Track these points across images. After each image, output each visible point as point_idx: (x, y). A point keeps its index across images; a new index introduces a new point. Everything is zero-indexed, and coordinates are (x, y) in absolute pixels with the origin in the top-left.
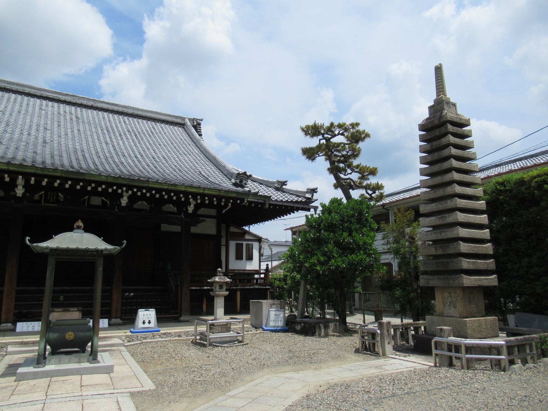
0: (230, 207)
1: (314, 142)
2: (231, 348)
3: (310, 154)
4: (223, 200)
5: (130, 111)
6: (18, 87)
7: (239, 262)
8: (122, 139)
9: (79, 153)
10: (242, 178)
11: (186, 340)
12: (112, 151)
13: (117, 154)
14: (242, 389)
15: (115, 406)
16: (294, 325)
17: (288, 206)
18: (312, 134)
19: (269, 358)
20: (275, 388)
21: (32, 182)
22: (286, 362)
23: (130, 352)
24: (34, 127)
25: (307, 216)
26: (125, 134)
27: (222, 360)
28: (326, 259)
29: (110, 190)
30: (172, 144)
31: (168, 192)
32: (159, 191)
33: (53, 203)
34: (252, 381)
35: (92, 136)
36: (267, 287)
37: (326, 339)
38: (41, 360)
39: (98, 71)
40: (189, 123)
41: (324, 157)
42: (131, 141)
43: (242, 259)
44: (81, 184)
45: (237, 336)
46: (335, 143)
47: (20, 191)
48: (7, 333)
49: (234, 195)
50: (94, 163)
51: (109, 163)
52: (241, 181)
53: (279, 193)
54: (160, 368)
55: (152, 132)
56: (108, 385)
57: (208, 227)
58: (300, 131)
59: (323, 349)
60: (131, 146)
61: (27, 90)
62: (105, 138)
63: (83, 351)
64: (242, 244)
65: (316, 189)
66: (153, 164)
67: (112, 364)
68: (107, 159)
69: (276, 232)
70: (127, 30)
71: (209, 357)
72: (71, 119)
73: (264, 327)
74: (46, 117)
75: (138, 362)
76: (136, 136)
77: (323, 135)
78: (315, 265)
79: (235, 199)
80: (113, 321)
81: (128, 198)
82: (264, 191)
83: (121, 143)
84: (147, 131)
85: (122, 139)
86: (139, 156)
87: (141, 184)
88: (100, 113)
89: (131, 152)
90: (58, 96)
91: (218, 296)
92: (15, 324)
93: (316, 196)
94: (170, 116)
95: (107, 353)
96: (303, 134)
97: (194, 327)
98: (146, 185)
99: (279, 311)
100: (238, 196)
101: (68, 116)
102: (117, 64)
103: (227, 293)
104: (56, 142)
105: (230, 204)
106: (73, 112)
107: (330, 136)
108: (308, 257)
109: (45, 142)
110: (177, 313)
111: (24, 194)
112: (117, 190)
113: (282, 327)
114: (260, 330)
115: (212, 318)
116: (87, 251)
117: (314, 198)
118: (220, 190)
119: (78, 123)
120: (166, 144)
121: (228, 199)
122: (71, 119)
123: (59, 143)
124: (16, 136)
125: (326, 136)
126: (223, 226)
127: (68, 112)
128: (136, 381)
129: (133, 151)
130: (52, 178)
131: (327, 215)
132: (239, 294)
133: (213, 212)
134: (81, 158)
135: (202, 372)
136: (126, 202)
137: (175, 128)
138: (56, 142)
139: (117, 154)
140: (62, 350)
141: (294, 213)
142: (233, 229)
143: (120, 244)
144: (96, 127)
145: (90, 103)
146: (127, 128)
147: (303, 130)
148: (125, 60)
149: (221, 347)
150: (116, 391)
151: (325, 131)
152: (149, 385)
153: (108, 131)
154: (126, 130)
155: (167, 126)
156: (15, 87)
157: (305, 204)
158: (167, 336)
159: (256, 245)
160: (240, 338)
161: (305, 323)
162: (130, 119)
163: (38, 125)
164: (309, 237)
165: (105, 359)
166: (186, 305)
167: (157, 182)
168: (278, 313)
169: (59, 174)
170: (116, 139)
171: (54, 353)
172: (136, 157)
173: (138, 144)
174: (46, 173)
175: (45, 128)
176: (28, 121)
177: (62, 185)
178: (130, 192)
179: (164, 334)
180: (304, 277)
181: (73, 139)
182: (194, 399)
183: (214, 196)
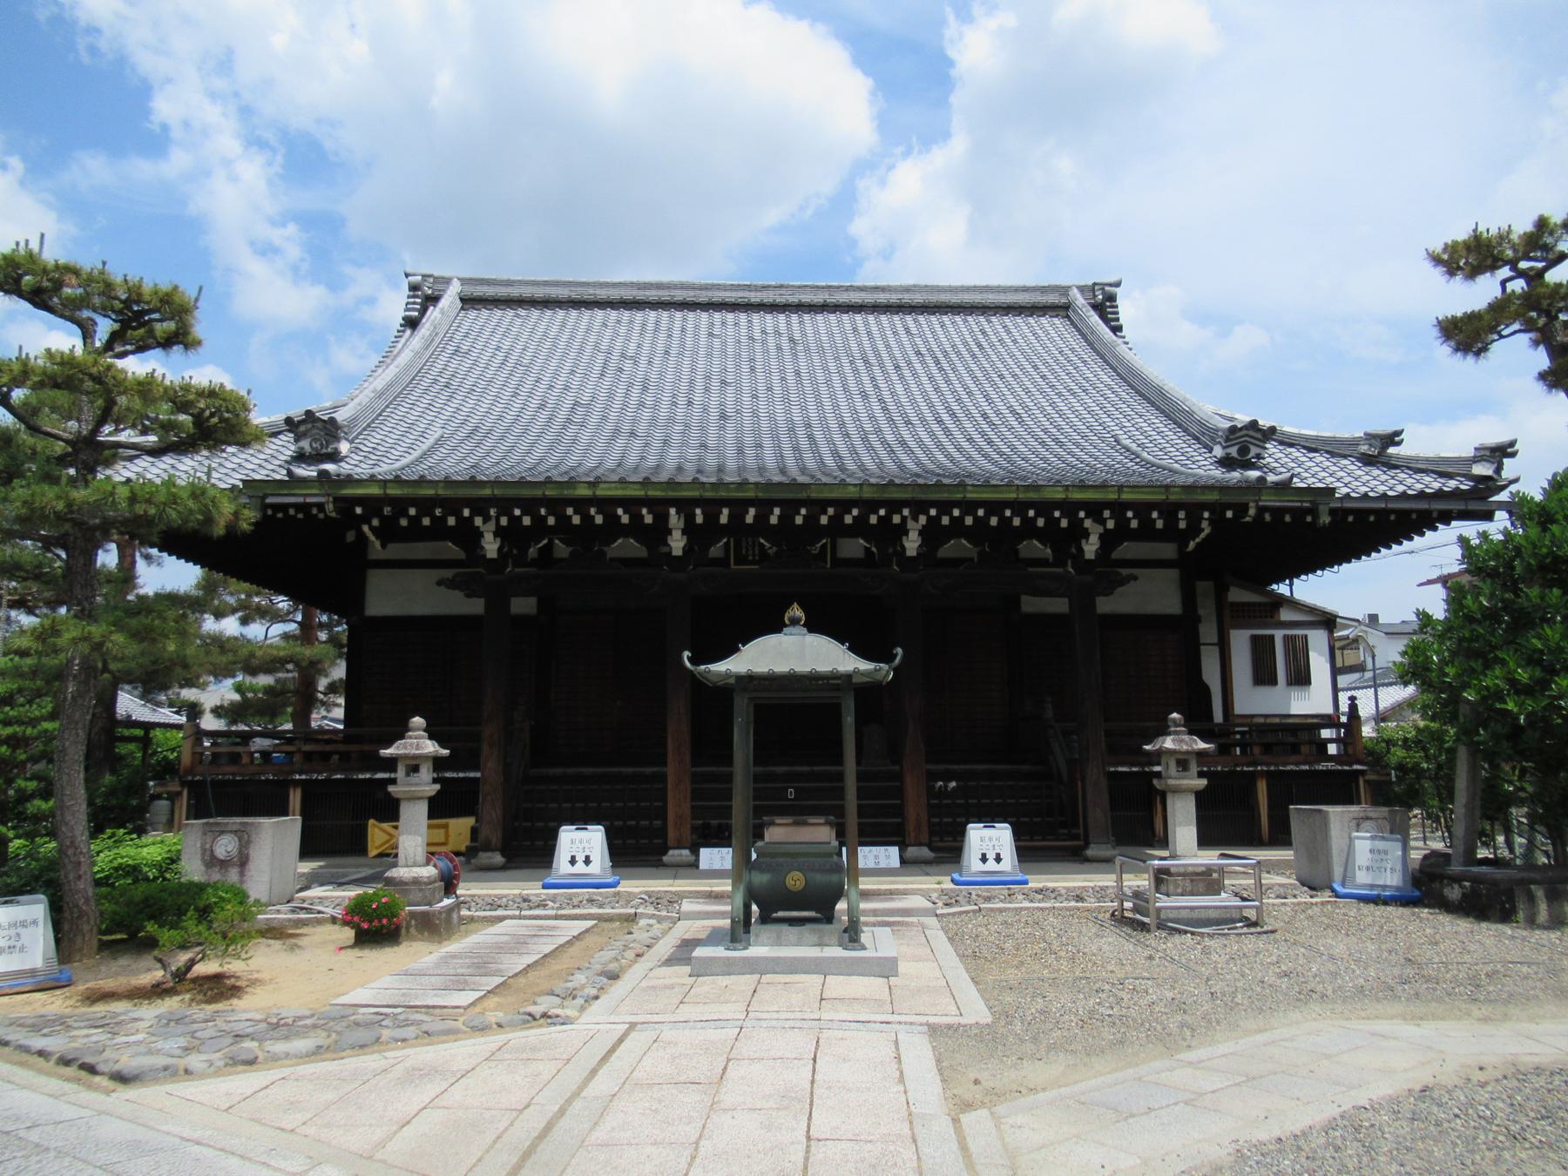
0: (1207, 531)
1: (1481, 292)
2: (1223, 940)
3: (1468, 335)
4: (1182, 515)
5: (918, 298)
6: (661, 293)
7: (1265, 691)
8: (902, 377)
9: (801, 432)
10: (1246, 441)
11: (1099, 910)
12: (879, 413)
13: (891, 420)
14: (1223, 1048)
15: (889, 1051)
16: (1436, 885)
17: (1408, 512)
18: (1468, 269)
19: (1334, 975)
20: (1328, 1057)
21: (699, 519)
22: (1387, 992)
23: (946, 932)
24: (700, 384)
25: (1463, 541)
26: (909, 363)
27: (1188, 968)
28: (1538, 673)
29: (873, 519)
30: (1035, 367)
31: (1019, 507)
32: (994, 507)
33: (753, 562)
34: (1260, 1031)
35: (828, 382)
36: (1356, 767)
37: (1554, 936)
38: (740, 931)
39: (845, 201)
40: (1080, 300)
41: (1524, 339)
42: (924, 380)
43: (1272, 681)
44: (803, 511)
45: (1241, 908)
46: (1559, 285)
47: (677, 543)
48: (681, 871)
49: (1213, 497)
50: (836, 454)
51: (870, 448)
52: (1244, 450)
53: (1376, 472)
54: (1013, 975)
55: (980, 346)
56: (879, 1002)
57: (1153, 594)
58: (1428, 266)
59: (1529, 964)
60: (924, 394)
61: (679, 295)
62: (859, 382)
63: (828, 917)
64: (1272, 637)
65: (1512, 444)
66: (983, 434)
67: (894, 954)
68: (865, 439)
69: (1395, 589)
70: (909, 73)
71: (1151, 958)
72: (779, 348)
73: (1337, 887)
74: (724, 352)
75: (962, 957)
76: (937, 362)
77: (1513, 264)
78: (1499, 696)
79: (1217, 509)
80: (912, 851)
81: (921, 533)
82: (1313, 472)
83: (899, 388)
84: (966, 344)
85: (902, 377)
86: (945, 417)
87: (945, 496)
88: (845, 317)
89: (926, 412)
90: (746, 294)
91: (1177, 791)
92: (696, 853)
93: (1510, 468)
94: (1026, 289)
95: (888, 929)
96: (1438, 273)
97: (1114, 877)
98: (959, 496)
99: (1383, 838)
100: (1227, 499)
101: (771, 341)
102: (891, 167)
103: (1204, 782)
104: (747, 414)
105: (1205, 524)
106: (783, 327)
107: (1540, 265)
108: (1474, 671)
109: (723, 416)
110: (1076, 837)
111: (687, 550)
112: (888, 517)
113: (1397, 888)
114: (1325, 896)
115: (1165, 853)
116: (814, 679)
117: (1504, 474)
118: (1167, 487)
119: (795, 355)
120: (1017, 371)
121: (1194, 510)
122: (779, 348)
123: (755, 414)
124: (664, 412)
125: (1523, 265)
126: (1204, 587)
127: (770, 330)
128: (949, 1000)
129: (931, 406)
130: (738, 506)
131: (1534, 532)
132: (1262, 787)
133: (1168, 550)
134: (804, 443)
135: (1123, 994)
136: (916, 545)
137: (1043, 320)
138: (747, 414)
139: (891, 420)
140: (781, 914)
141: (1435, 529)
142: (1237, 595)
143: (888, 658)
144: (837, 359)
145: (819, 298)
146: (914, 345)
147: (1436, 260)
148: (907, 153)
149: (1193, 933)
150: (896, 1018)
151: (1515, 251)
152: (976, 1011)
153: (866, 362)
154: (911, 353)
155: (1019, 320)
156: (654, 292)
157: (1475, 499)
158: (1046, 899)
159: (1317, 642)
160: (1251, 914)
161: (1476, 880)
162: (921, 318)
163: (708, 378)
164: (1474, 607)
165: (878, 941)
166: (1098, 813)
167: (987, 485)
168: (1380, 845)
169: (751, 494)
170: (887, 380)
171: (765, 919)
172: (940, 422)
173: (943, 386)
174: (723, 494)
175: (723, 382)
176: (686, 370)
177: (762, 518)
178: (923, 519)
179: (1040, 891)
180: (1466, 733)
181: (786, 399)
182: (1086, 1059)
183: (1152, 506)
